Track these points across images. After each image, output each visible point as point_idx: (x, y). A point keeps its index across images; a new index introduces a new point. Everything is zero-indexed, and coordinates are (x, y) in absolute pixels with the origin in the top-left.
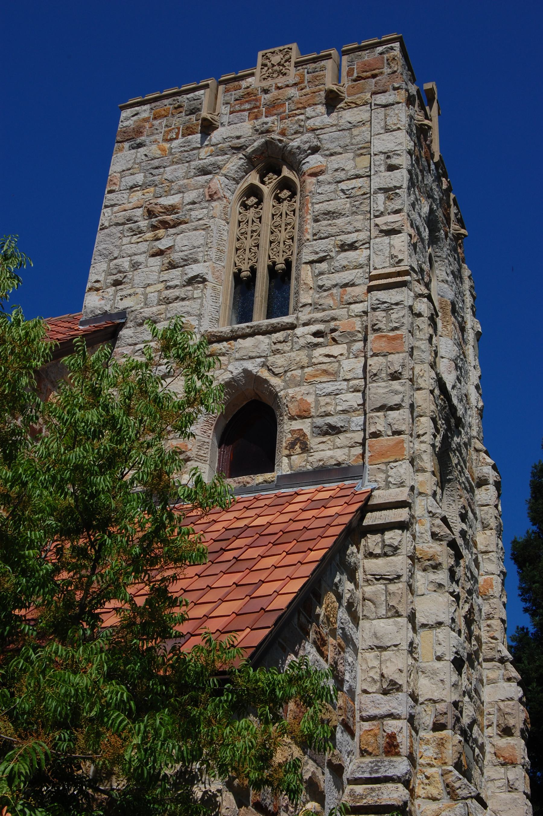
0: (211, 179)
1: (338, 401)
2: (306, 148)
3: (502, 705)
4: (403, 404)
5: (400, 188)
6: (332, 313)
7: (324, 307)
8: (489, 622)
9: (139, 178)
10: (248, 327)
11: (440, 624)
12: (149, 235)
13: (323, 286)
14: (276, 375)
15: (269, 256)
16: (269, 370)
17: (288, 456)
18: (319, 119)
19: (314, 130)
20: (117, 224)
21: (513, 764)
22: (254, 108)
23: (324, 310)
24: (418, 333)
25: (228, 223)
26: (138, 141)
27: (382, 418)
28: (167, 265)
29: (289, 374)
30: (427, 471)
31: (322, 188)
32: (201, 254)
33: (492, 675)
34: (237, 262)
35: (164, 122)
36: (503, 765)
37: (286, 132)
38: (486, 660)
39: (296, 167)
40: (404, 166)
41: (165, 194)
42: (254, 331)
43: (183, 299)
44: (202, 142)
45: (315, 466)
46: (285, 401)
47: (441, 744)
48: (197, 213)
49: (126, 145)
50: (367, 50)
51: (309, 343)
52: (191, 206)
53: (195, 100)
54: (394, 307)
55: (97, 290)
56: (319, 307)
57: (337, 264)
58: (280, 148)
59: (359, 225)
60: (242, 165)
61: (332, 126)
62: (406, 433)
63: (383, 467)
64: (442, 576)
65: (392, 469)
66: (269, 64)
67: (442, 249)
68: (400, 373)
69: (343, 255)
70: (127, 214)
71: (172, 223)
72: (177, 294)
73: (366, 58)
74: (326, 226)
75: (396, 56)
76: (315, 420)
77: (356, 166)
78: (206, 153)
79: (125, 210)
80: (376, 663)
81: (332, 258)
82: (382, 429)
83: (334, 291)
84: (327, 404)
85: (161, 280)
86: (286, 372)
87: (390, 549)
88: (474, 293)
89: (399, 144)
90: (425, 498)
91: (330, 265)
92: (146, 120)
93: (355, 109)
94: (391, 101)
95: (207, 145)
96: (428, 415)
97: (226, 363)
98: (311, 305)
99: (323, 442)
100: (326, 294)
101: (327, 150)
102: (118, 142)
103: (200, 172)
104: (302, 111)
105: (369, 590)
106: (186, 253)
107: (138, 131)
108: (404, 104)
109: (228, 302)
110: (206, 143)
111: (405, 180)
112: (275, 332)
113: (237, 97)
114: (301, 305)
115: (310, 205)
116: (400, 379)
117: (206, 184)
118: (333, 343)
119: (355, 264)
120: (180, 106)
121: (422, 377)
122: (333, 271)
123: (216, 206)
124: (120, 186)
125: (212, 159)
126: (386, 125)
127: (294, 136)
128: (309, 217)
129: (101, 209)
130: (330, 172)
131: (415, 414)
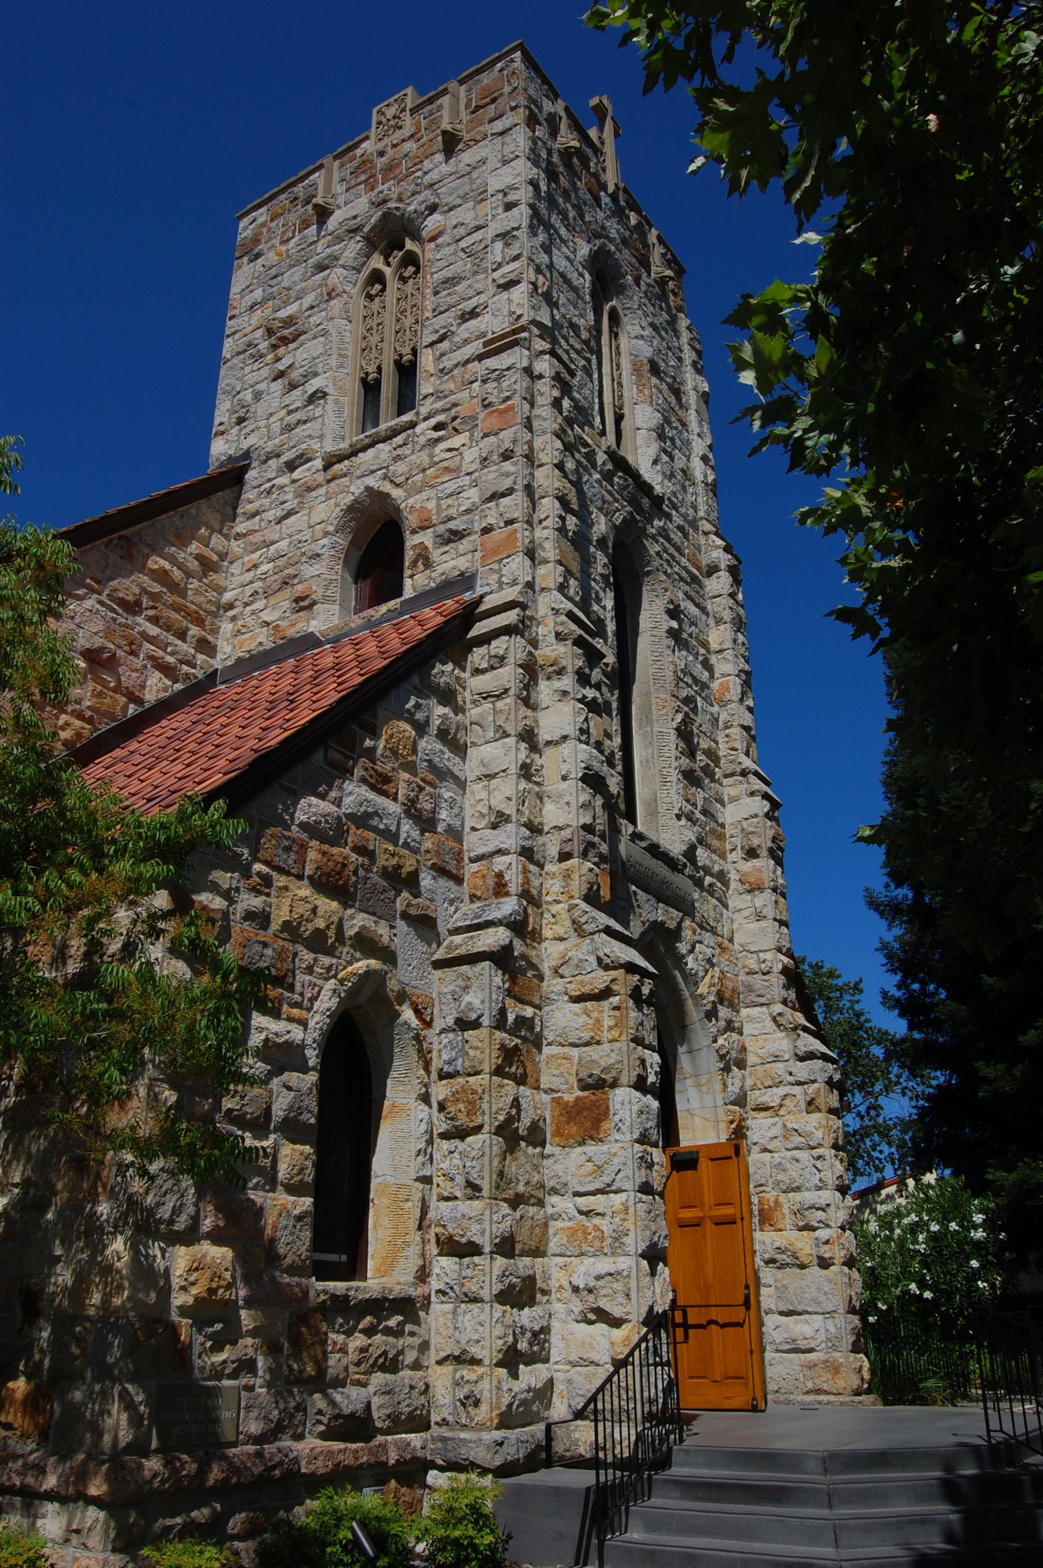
3: (745, 824)
5: (518, 229)
6: (452, 399)
8: (727, 731)
9: (258, 294)
11: (565, 738)
14: (398, 485)
17: (411, 576)
18: (436, 171)
20: (239, 353)
21: (760, 889)
23: (446, 397)
27: (494, 509)
33: (733, 792)
36: (749, 892)
38: (726, 776)
39: (416, 237)
43: (305, 422)
47: (567, 876)
49: (245, 259)
55: (222, 433)
59: (479, 286)
63: (496, 566)
64: (567, 682)
66: (384, 120)
67: (631, 299)
80: (484, 795)
81: (453, 333)
82: (492, 521)
83: (456, 372)
88: (698, 346)
91: (451, 342)
92: (263, 225)
105: (474, 713)
107: (256, 241)
112: (395, 436)
120: (296, 199)
131: (537, 496)
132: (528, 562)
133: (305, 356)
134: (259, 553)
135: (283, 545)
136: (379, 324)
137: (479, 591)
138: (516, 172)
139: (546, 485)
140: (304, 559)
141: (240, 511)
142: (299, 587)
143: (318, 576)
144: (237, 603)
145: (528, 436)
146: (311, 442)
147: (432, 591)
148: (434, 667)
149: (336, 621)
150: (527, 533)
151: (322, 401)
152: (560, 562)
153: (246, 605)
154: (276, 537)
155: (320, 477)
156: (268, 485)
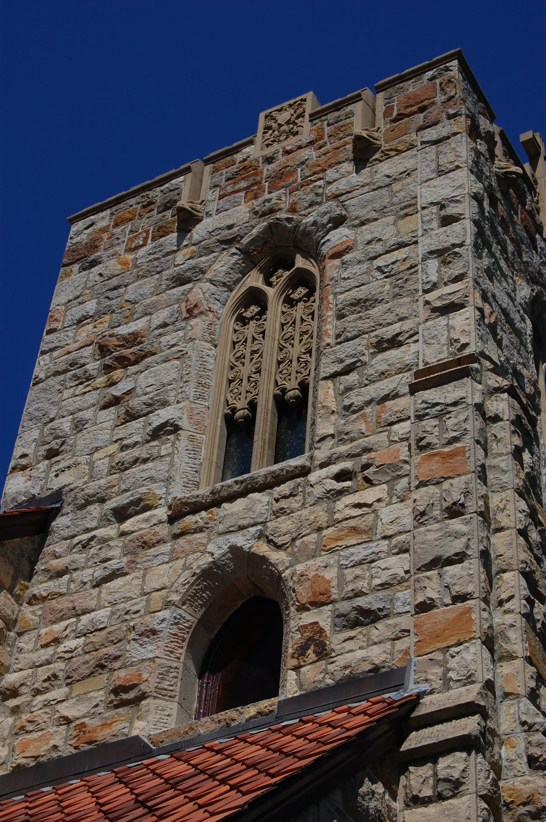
0: (191, 289)
1: (374, 571)
2: (325, 221)
4: (469, 553)
5: (461, 245)
6: (363, 442)
7: (352, 435)
9: (91, 306)
10: (236, 482)
12: (101, 380)
13: (351, 406)
14: (279, 547)
15: (276, 382)
16: (270, 541)
17: (297, 668)
18: (344, 181)
19: (336, 197)
20: (57, 373)
22: (253, 185)
23: (352, 440)
24: (494, 446)
25: (216, 346)
26: (92, 257)
28: (123, 416)
29: (298, 543)
30: (517, 657)
31: (349, 271)
32: (173, 393)
34: (230, 399)
35: (129, 226)
37: (298, 206)
40: (467, 216)
41: (126, 320)
42: (246, 487)
44: (179, 242)
45: (338, 677)
46: (291, 584)
48: (168, 338)
49: (76, 267)
50: (411, 79)
51: (329, 492)
52: (161, 330)
53: (171, 191)
54: (450, 409)
55: (24, 468)
56: (346, 437)
57: (371, 371)
58: (290, 230)
59: (403, 311)
60: (236, 263)
61: (363, 186)
62: (475, 596)
63: (439, 656)
65: (453, 657)
66: (274, 125)
68: (462, 505)
69: (380, 357)
70: (70, 357)
71: (132, 358)
72: (136, 454)
73: (411, 90)
74: (355, 320)
75: (453, 77)
76: (337, 606)
77: (399, 232)
78: (184, 256)
79: (69, 353)
81: (364, 364)
82: (434, 595)
83: (368, 410)
84: (356, 577)
85: (115, 438)
86: (294, 540)
87: (447, 785)
89: (458, 187)
90: (515, 701)
91: (361, 375)
92: (104, 230)
93: (397, 157)
94: (445, 134)
95: (186, 246)
96: (515, 567)
97: (205, 541)
98: (333, 436)
99: (351, 638)
100: (355, 416)
101: (357, 218)
102: (64, 265)
103: (175, 282)
104: (321, 175)
106: (152, 394)
107: (93, 246)
108: (464, 134)
109: (215, 456)
110: (185, 243)
111: (468, 234)
112: (278, 485)
113: (229, 175)
114: (317, 439)
115: (331, 297)
116: (463, 514)
117: (183, 297)
118: (367, 485)
119: (398, 366)
120: (151, 203)
121: (503, 510)
122: (366, 382)
123: (197, 324)
124: (63, 322)
125: (192, 262)
126: (439, 166)
127: (309, 210)
128: (329, 313)
129: (36, 357)
130: (360, 247)
131: (494, 569)
132: (487, 654)
133: (151, 381)
134: (64, 624)
135: (102, 614)
136: (253, 352)
137: (412, 689)
138: (457, 184)
139: (508, 554)
140: (132, 635)
141: (39, 567)
142: (122, 673)
143: (152, 660)
144: (24, 689)
145: (483, 490)
146: (153, 486)
147: (328, 689)
148: (361, 784)
149: (172, 724)
150: (485, 615)
151: (172, 437)
152: (529, 660)
153: (38, 692)
154: (92, 604)
155: (164, 531)
156: (85, 537)
